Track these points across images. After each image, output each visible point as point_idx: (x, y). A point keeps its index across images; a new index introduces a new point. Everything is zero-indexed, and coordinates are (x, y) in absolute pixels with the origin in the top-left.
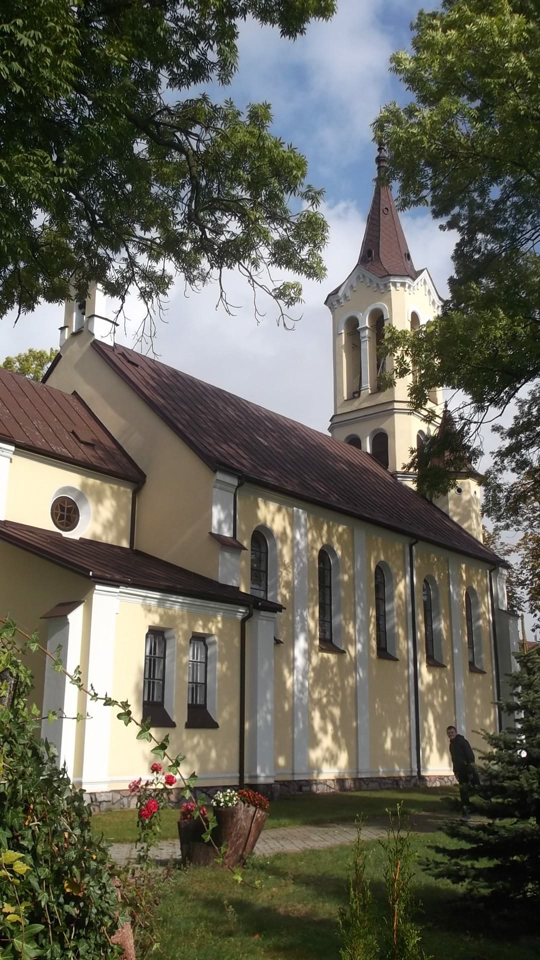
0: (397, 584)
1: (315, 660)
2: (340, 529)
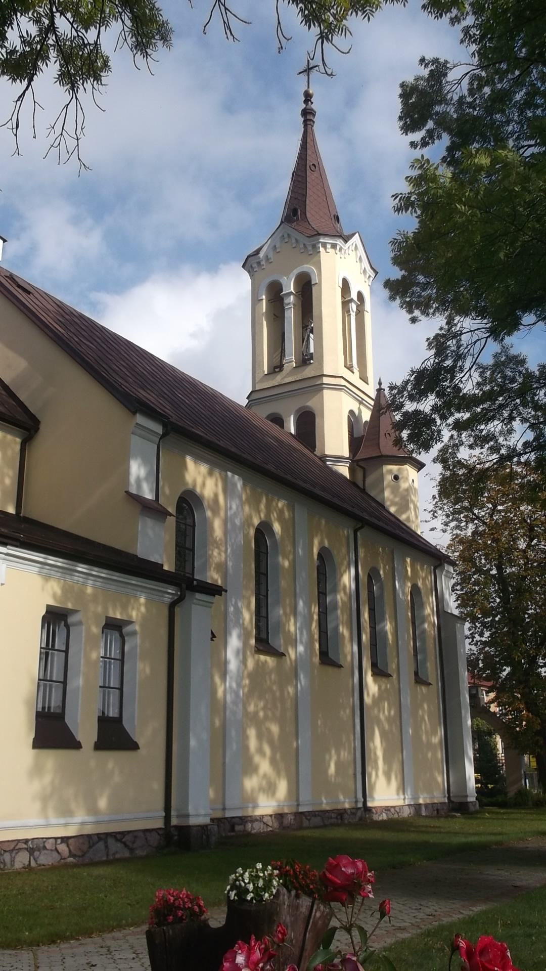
0: (342, 575)
1: (250, 664)
2: (280, 505)
